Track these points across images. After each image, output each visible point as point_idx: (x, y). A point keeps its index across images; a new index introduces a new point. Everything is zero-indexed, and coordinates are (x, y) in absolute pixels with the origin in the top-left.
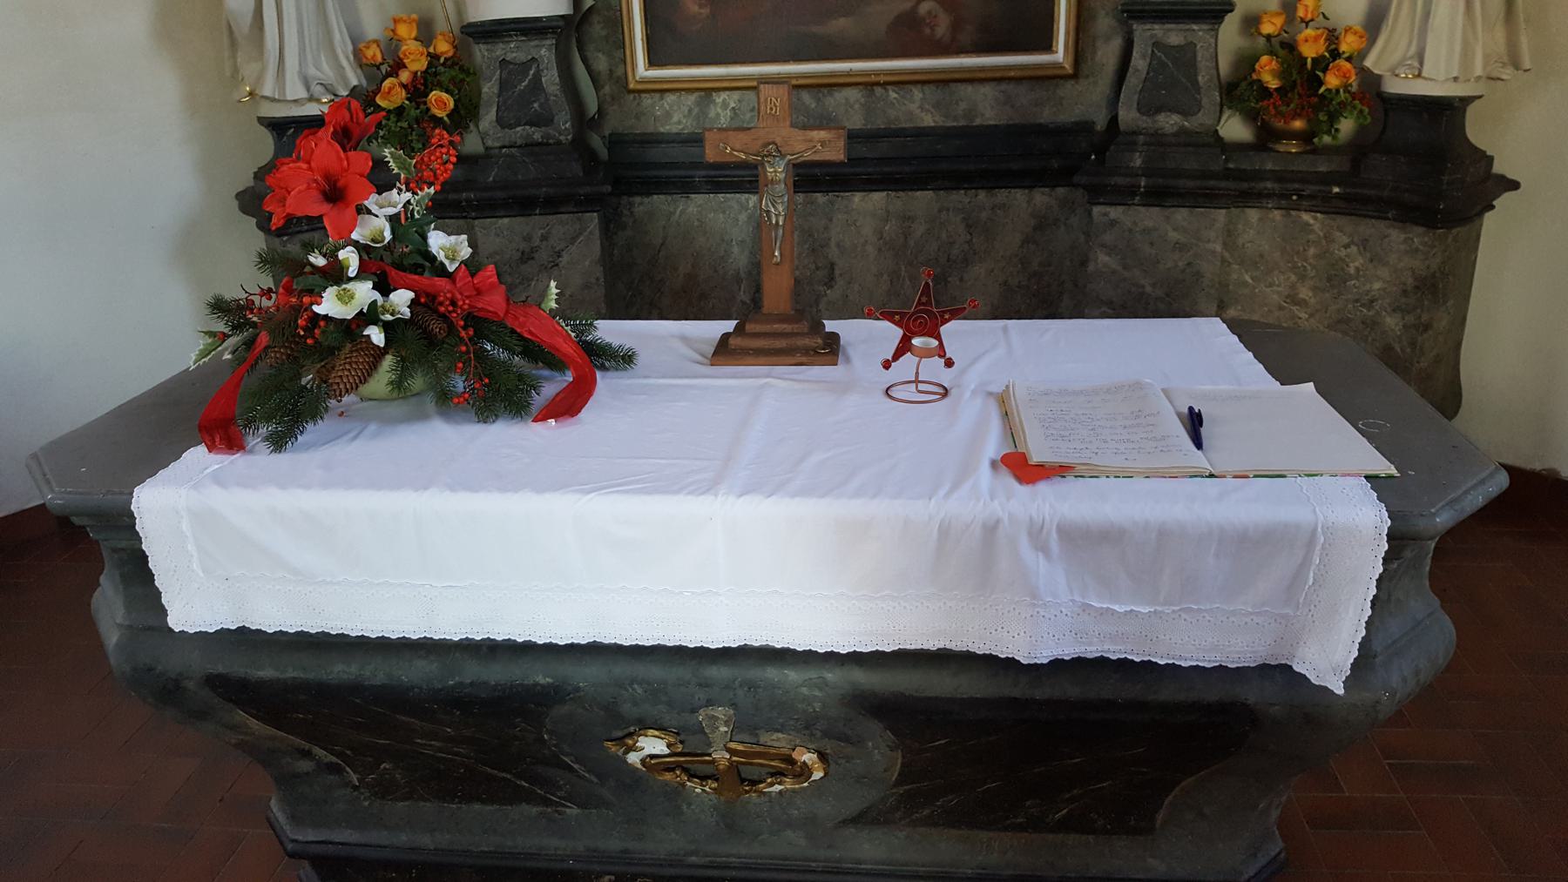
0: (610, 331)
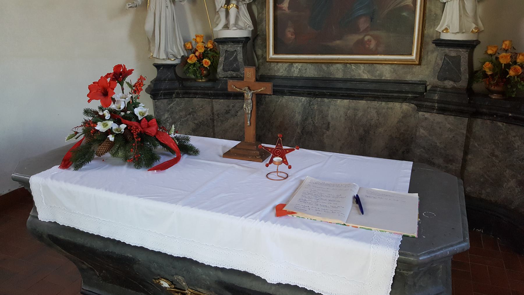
0: (195, 141)
